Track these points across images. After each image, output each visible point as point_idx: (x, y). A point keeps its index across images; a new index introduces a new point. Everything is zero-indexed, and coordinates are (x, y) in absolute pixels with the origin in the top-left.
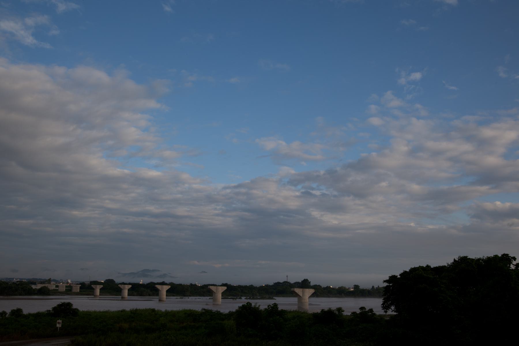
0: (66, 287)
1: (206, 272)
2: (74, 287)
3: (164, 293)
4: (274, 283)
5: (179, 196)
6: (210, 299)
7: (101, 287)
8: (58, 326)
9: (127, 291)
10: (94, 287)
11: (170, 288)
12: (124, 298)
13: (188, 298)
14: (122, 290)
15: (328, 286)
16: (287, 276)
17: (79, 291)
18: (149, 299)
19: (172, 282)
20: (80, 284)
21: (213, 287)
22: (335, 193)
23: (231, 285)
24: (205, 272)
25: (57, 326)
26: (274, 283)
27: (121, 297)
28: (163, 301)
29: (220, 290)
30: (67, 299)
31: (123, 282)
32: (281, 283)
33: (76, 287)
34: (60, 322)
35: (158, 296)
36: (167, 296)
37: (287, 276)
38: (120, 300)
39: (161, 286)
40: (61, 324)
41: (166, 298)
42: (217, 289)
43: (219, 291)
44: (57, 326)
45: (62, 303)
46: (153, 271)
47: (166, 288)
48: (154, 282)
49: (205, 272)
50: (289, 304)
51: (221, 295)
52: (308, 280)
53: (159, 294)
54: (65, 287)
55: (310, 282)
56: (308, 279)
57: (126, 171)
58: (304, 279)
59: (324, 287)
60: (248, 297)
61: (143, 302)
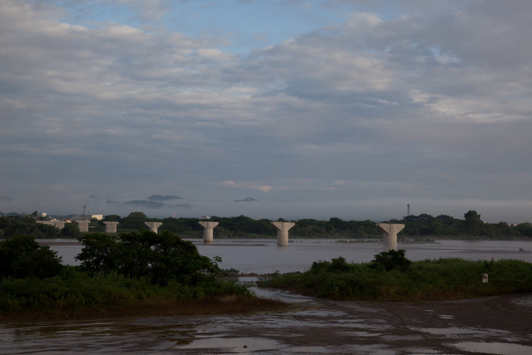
0: (89, 226)
1: (257, 201)
2: (108, 226)
3: (286, 234)
4: (404, 217)
5: (178, 70)
6: (336, 242)
7: (159, 226)
8: (484, 282)
9: (212, 231)
10: (149, 225)
11: (294, 226)
12: (209, 242)
13: (301, 241)
14: (204, 230)
15: (502, 222)
16: (408, 206)
17: (116, 231)
18: (237, 243)
19: (246, 215)
20: (292, 221)
21: (384, 224)
22: (456, 60)
23: (343, 220)
24: (251, 199)
25: (483, 282)
26: (404, 217)
27: (202, 240)
28: (286, 246)
29: (395, 229)
30: (238, 245)
31: (181, 217)
32: (417, 216)
33: (112, 225)
34: (486, 276)
35: (276, 238)
36: (289, 237)
37: (408, 206)
38: (203, 245)
39: (281, 223)
40: (487, 279)
41: (289, 241)
42: (390, 228)
43: (394, 231)
44: (483, 282)
45: (390, 251)
46: (168, 198)
47: (288, 226)
48: (218, 216)
49: (251, 199)
50: (494, 251)
51: (396, 237)
52: (476, 213)
53: (204, 236)
54: (88, 225)
55: (479, 216)
56: (476, 211)
57: (80, 28)
58: (470, 211)
59: (302, 219)
60: (146, 237)
61: (254, 247)
